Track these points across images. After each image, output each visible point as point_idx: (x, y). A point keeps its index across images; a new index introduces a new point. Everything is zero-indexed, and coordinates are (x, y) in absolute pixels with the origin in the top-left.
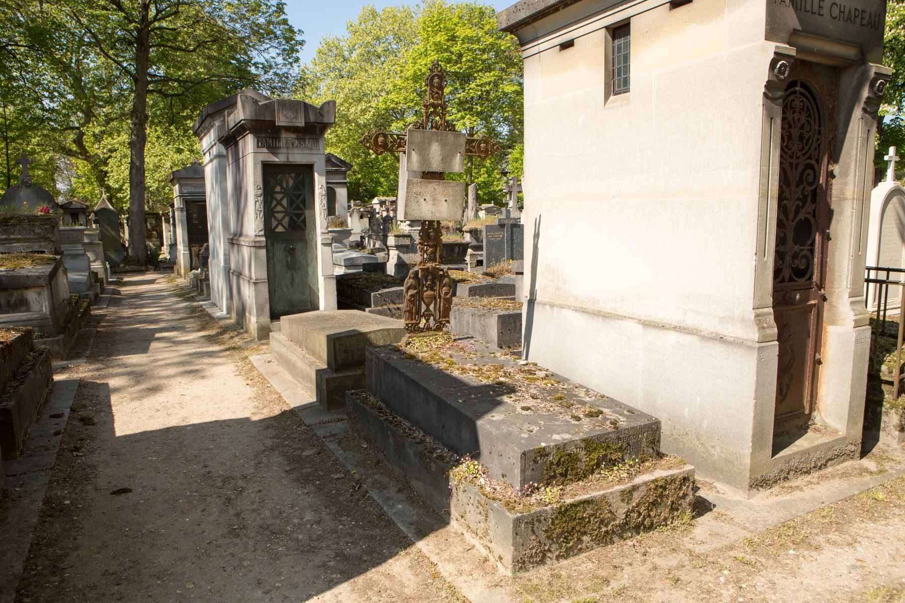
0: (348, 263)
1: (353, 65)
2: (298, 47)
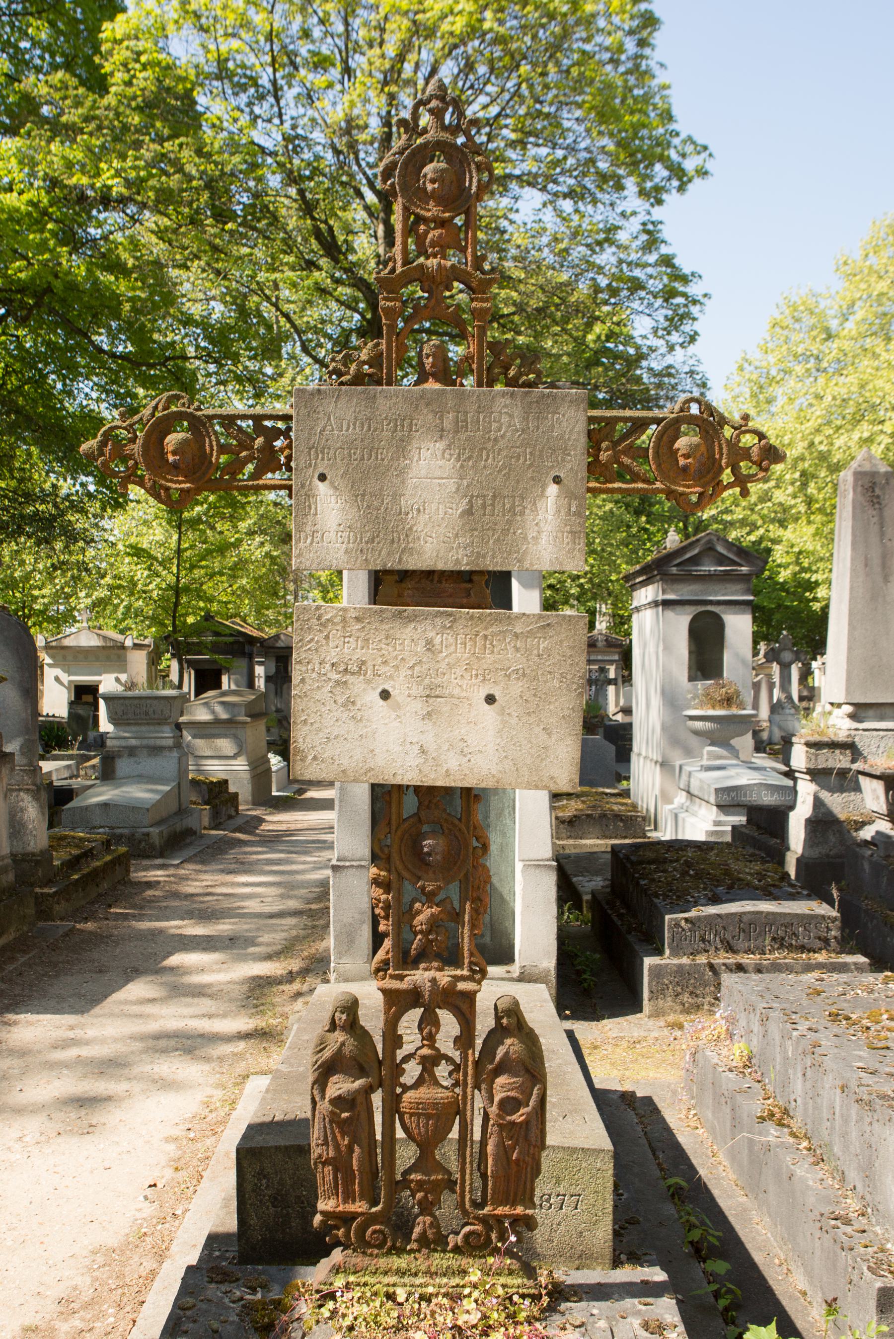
0: (726, 799)
1: (847, 345)
2: (695, 310)
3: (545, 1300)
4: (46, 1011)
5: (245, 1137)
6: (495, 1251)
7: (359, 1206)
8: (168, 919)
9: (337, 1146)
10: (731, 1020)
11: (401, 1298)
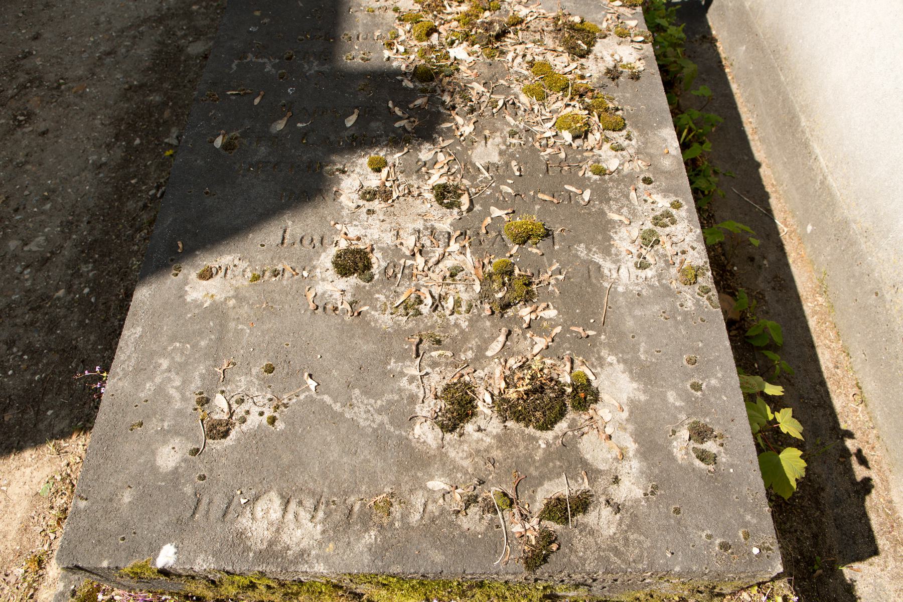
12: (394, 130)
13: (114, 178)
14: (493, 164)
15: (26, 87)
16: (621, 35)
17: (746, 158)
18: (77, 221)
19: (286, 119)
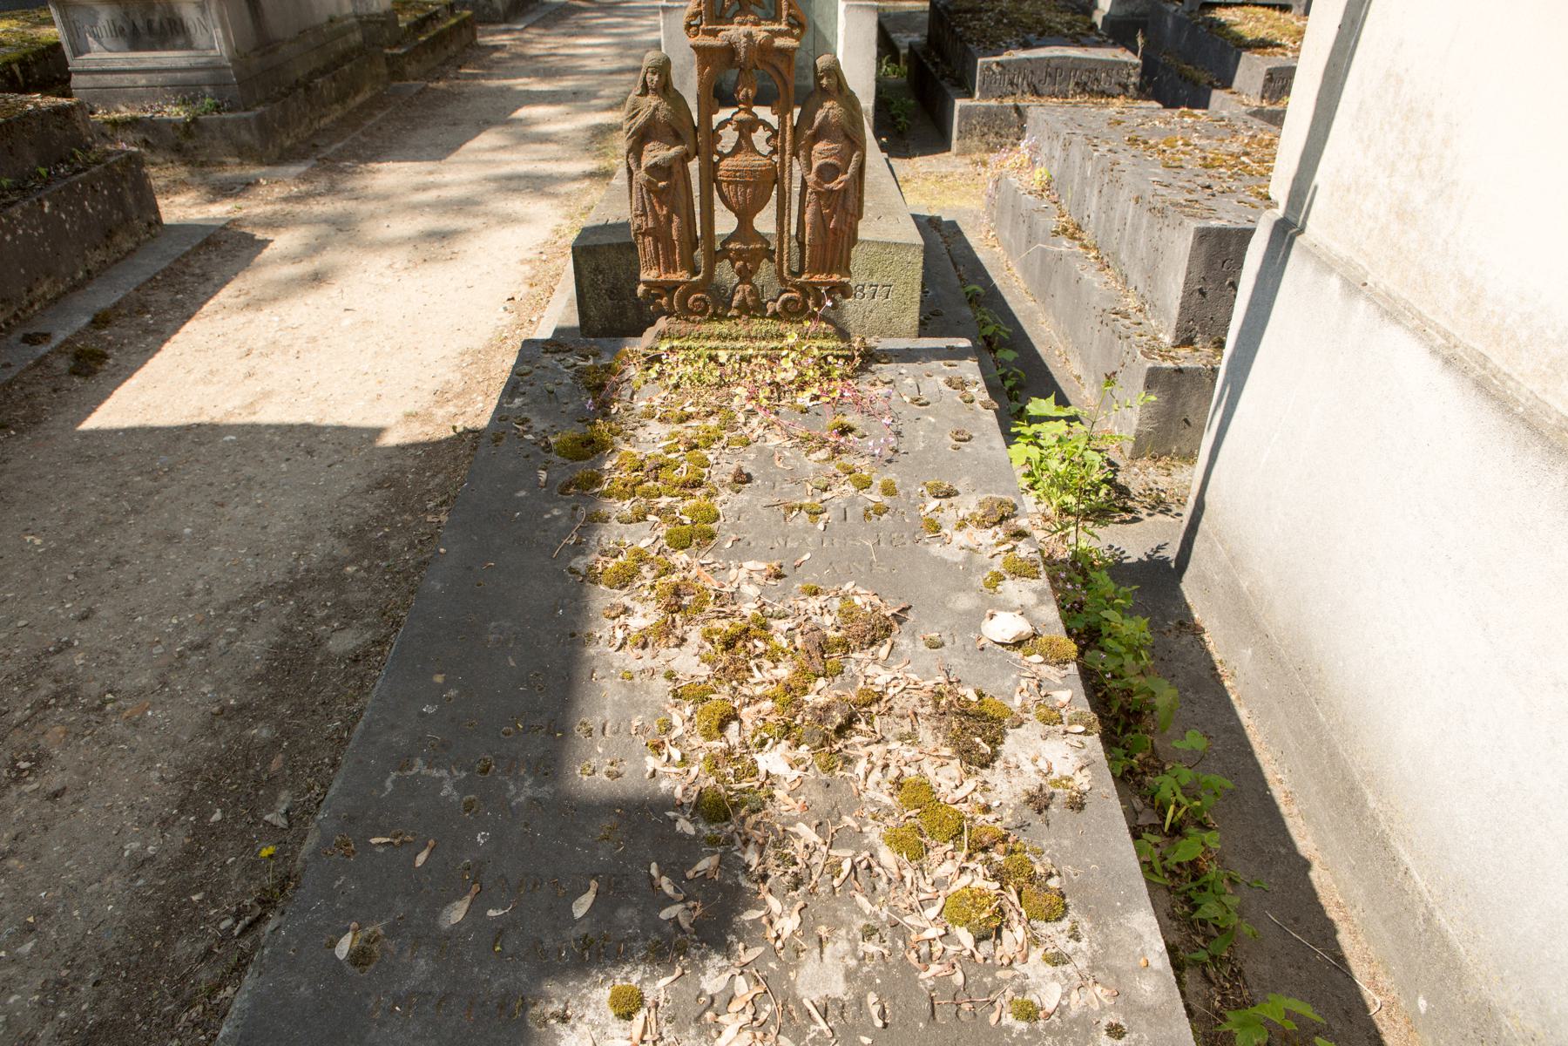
3: (858, 361)
4: (406, 160)
5: (579, 237)
6: (813, 316)
7: (681, 276)
8: (515, 77)
9: (656, 217)
10: (1034, 149)
11: (723, 359)
12: (659, 926)
13: (161, 888)
14: (835, 1000)
15: (46, 706)
16: (1046, 721)
17: (1283, 851)
18: (76, 979)
19: (468, 898)
